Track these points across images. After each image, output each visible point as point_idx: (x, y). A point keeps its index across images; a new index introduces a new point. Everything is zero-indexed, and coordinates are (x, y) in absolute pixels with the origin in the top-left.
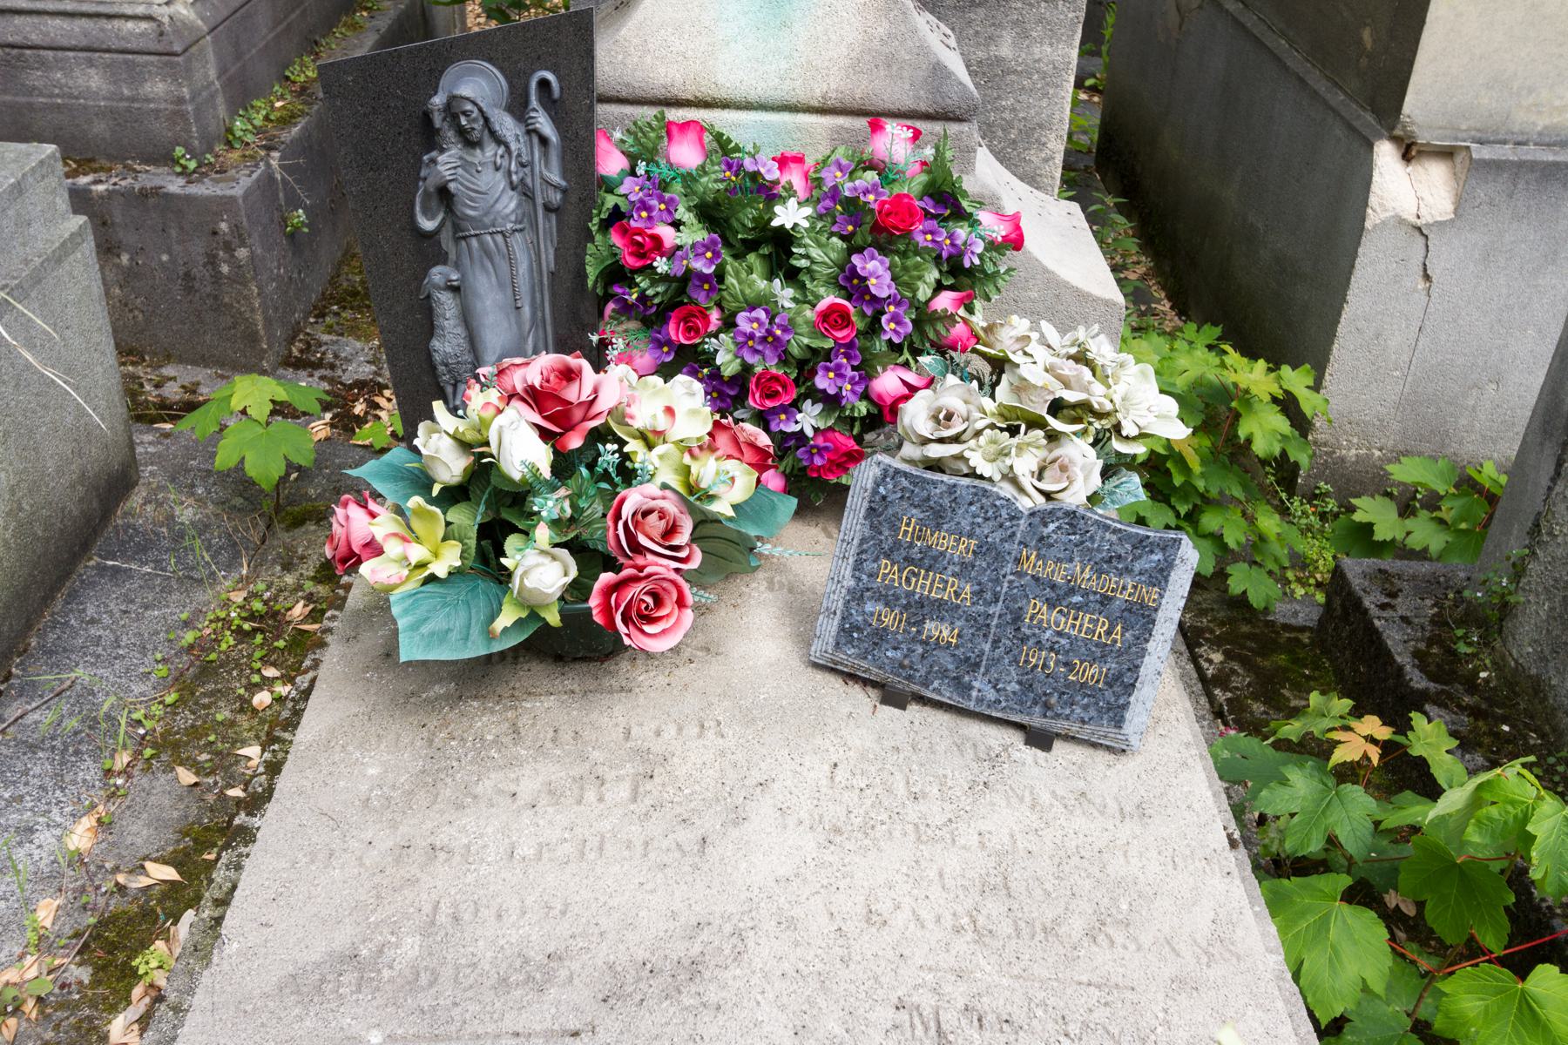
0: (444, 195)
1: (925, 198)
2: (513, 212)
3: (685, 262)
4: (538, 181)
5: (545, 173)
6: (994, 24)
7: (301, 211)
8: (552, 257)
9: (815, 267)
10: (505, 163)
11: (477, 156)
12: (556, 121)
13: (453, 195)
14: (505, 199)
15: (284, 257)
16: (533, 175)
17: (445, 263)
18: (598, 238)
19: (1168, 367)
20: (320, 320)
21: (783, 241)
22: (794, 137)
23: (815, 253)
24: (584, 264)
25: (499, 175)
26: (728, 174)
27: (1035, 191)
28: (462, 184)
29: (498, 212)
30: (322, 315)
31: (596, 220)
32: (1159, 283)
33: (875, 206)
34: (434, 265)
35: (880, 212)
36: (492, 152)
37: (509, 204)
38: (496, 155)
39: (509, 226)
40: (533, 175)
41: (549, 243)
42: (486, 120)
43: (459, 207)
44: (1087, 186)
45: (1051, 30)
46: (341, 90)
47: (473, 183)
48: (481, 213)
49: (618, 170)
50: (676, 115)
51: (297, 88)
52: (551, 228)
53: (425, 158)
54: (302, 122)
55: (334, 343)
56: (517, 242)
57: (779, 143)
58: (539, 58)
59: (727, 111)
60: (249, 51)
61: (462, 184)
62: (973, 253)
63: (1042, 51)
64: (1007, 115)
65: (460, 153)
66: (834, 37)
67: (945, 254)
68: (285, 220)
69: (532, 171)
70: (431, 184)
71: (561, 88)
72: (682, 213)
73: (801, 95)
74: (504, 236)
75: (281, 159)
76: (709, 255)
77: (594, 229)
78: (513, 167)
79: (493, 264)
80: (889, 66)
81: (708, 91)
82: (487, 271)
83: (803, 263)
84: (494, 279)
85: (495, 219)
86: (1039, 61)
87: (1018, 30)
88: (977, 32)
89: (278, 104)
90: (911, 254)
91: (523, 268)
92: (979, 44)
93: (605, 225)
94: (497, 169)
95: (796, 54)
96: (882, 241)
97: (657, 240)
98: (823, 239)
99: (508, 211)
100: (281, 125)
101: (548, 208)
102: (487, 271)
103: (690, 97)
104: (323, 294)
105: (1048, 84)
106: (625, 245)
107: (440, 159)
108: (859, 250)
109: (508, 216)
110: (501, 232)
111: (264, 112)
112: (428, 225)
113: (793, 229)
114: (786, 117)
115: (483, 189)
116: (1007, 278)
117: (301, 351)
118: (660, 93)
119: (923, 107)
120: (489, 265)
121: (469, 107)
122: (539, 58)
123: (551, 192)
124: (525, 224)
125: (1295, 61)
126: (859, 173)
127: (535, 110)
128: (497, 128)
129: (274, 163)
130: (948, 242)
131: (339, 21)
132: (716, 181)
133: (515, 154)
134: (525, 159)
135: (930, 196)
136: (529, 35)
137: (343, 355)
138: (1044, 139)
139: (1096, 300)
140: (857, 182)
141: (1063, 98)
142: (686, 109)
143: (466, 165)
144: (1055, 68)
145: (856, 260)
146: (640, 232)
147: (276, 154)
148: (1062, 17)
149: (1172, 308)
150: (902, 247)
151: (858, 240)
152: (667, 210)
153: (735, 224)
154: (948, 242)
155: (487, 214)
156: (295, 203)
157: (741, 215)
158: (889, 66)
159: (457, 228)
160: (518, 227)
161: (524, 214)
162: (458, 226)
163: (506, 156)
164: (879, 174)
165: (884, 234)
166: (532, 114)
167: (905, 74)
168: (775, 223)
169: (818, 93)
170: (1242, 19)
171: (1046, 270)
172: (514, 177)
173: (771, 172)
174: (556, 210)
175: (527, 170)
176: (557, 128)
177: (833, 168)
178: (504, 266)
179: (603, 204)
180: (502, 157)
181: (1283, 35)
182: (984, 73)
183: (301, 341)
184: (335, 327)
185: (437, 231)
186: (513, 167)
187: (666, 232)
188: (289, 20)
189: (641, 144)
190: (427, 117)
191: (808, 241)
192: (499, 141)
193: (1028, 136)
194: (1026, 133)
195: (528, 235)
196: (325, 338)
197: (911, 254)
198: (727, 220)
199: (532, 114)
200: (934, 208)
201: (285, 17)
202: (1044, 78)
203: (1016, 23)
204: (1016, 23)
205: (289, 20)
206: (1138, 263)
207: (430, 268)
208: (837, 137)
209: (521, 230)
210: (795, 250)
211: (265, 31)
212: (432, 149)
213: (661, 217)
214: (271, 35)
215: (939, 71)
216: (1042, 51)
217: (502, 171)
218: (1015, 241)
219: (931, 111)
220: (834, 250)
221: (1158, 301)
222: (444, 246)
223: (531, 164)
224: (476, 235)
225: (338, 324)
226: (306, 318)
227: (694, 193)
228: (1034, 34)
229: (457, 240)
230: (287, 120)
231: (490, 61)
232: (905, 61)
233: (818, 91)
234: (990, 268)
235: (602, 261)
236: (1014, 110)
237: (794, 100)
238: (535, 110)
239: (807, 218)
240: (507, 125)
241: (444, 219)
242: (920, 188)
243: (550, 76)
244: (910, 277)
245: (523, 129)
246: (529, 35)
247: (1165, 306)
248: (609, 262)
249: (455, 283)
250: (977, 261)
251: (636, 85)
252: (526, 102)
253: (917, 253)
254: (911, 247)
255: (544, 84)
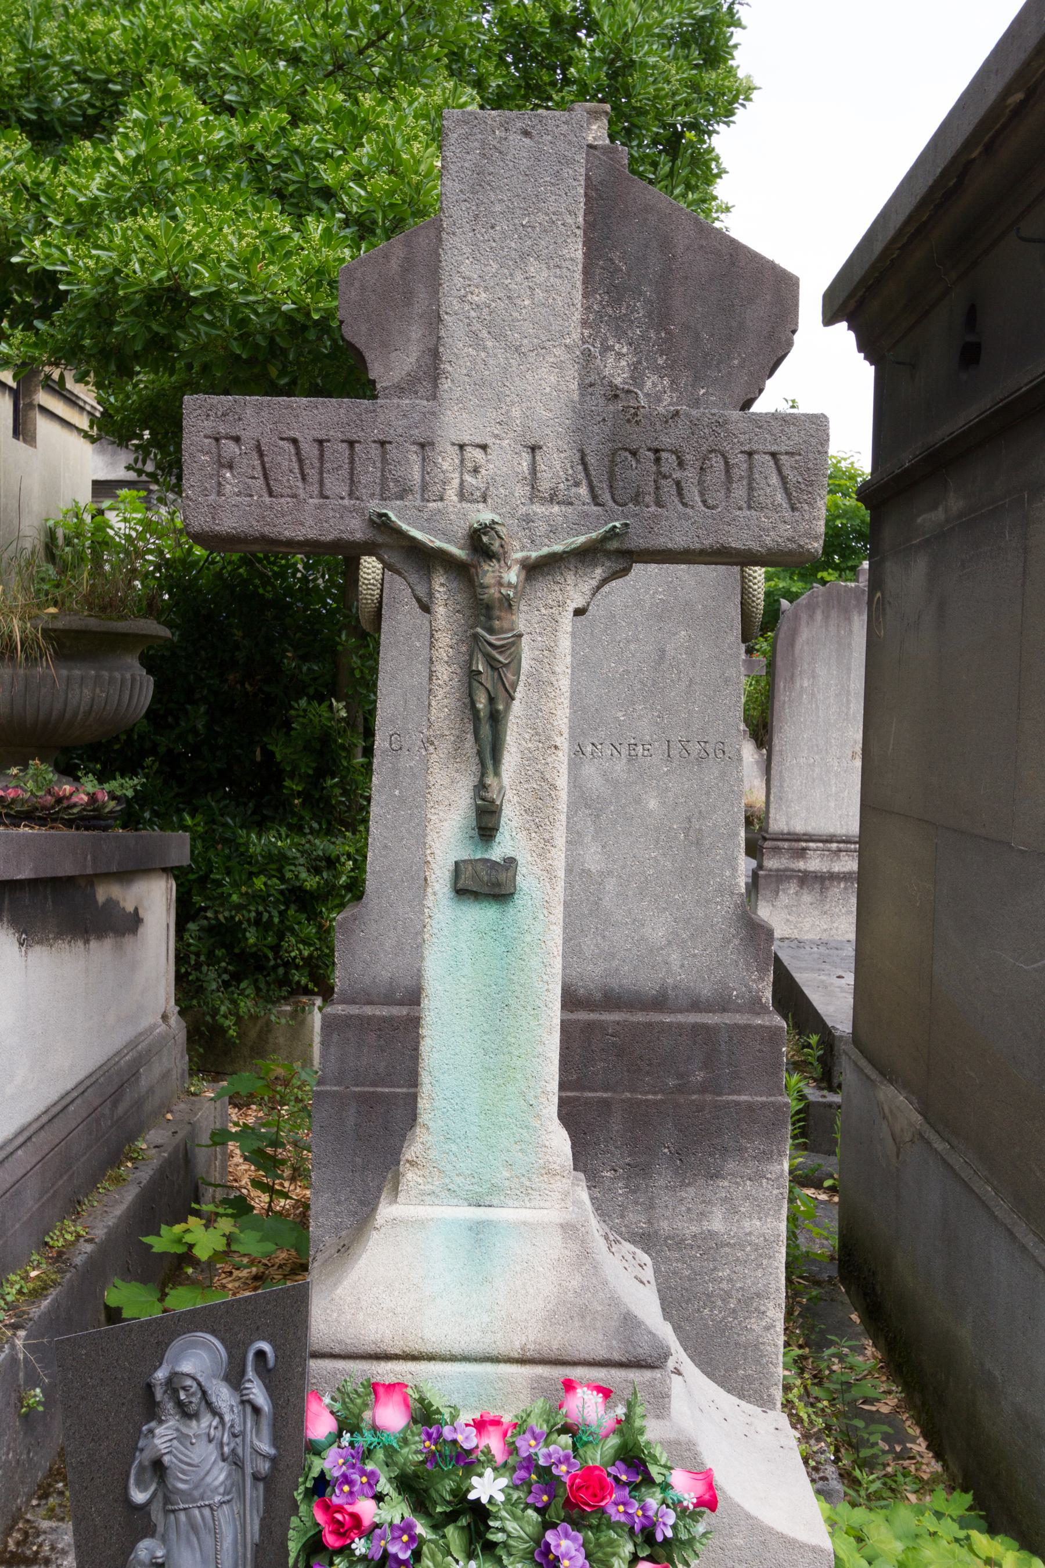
0: (158, 1467)
1: (617, 1463)
2: (221, 1484)
3: (383, 1543)
4: (248, 1450)
5: (256, 1442)
6: (704, 1202)
7: (38, 1390)
8: (257, 1527)
9: (511, 1542)
10: (219, 1434)
11: (194, 1428)
12: (270, 1389)
13: (166, 1468)
14: (215, 1471)
15: (15, 1440)
16: (244, 1445)
17: (152, 1536)
18: (303, 1508)
19: (913, 1559)
20: (43, 1502)
21: (480, 1512)
22: (497, 1386)
23: (511, 1526)
24: (287, 1539)
25: (212, 1446)
26: (427, 1443)
27: (743, 1403)
28: (176, 1457)
29: (209, 1485)
30: (45, 1496)
31: (301, 1489)
32: (912, 1417)
33: (566, 1479)
34: (142, 1538)
35: (571, 1487)
36: (208, 1423)
37: (220, 1475)
38: (210, 1426)
39: (217, 1498)
40: (244, 1445)
41: (255, 1512)
42: (204, 1393)
43: (171, 1480)
44: (832, 1300)
45: (758, 1206)
46: (74, 1363)
47: (190, 1458)
48: (191, 1486)
49: (326, 1433)
50: (386, 1372)
51: (53, 1254)
52: (257, 1497)
53: (145, 1428)
54: (53, 1293)
55: (54, 1530)
56: (224, 1515)
57: (483, 1392)
58: (258, 1328)
59: (433, 1362)
60: (13, 1226)
61: (176, 1457)
62: (665, 1524)
63: (753, 1225)
64: (724, 1285)
65: (177, 1424)
66: (531, 1291)
67: (637, 1527)
68: (21, 1400)
69: (244, 1440)
70: (144, 1458)
71: (276, 1357)
72: (384, 1486)
73: (502, 1347)
74: (212, 1509)
75: (27, 1338)
76: (405, 1538)
77: (299, 1498)
78: (225, 1439)
79: (198, 1539)
80: (583, 1317)
81: (414, 1345)
82: (192, 1548)
83: (499, 1537)
84: (198, 1555)
85: (204, 1492)
86: (750, 1234)
87: (728, 1206)
88: (689, 1209)
89: (33, 1274)
90: (604, 1528)
91: (227, 1543)
92: (691, 1220)
93: (309, 1493)
94: (210, 1441)
95: (496, 1308)
96: (575, 1516)
97: (356, 1518)
98: (519, 1512)
99: (217, 1483)
100: (32, 1299)
101: (256, 1477)
102: (192, 1548)
103: (398, 1352)
104: (51, 1469)
105: (761, 1256)
106: (326, 1523)
107: (157, 1431)
108: (554, 1526)
109: (217, 1488)
110: (209, 1505)
111: (18, 1287)
112: (139, 1497)
113: (490, 1502)
114: (488, 1368)
115: (196, 1460)
116: (704, 1541)
117: (18, 1544)
118: (371, 1349)
119: (616, 1356)
120: (195, 1540)
121: (189, 1382)
122: (258, 1328)
123: (260, 1460)
124: (234, 1494)
125: (1002, 1209)
126: (555, 1436)
127: (250, 1381)
128: (214, 1399)
129: (19, 1343)
130: (640, 1513)
131: (104, 1175)
132: (417, 1452)
133: (228, 1425)
134: (237, 1429)
135: (623, 1460)
136: (250, 1308)
137: (60, 1546)
138: (763, 1308)
139: (803, 1546)
140: (552, 1448)
141: (777, 1268)
142: (395, 1362)
143: (182, 1437)
144: (766, 1240)
145: (550, 1537)
146: (340, 1509)
147: (22, 1333)
148: (767, 1194)
149: (928, 1448)
150: (595, 1522)
151: (552, 1514)
152: (369, 1483)
153: (434, 1495)
154: (640, 1513)
155: (196, 1487)
156: (33, 1381)
157: (440, 1487)
158: (583, 1317)
159: (167, 1500)
160: (227, 1498)
161: (233, 1485)
162: (167, 1497)
163: (220, 1427)
164: (572, 1437)
165: (576, 1510)
166: (248, 1385)
167: (598, 1325)
168: (472, 1496)
169: (517, 1345)
170: (950, 1161)
171: (749, 1516)
172: (226, 1449)
173: (469, 1439)
174: (263, 1479)
175: (239, 1440)
176: (270, 1396)
177: (528, 1436)
178: (209, 1540)
179: (310, 1468)
180: (216, 1428)
181: (988, 1182)
182: (699, 1247)
183: (19, 1530)
184: (58, 1510)
185: (149, 1502)
186: (225, 1439)
187: (366, 1508)
188: (55, 1188)
189: (348, 1408)
190: (149, 1387)
191: (504, 1514)
192: (215, 1412)
193: (747, 1306)
194: (745, 1302)
195: (236, 1507)
196: (45, 1525)
197: (604, 1528)
198: (426, 1491)
199: (248, 1385)
200: (626, 1473)
201: (53, 1185)
202: (756, 1250)
203: (725, 1200)
204: (725, 1200)
205: (55, 1188)
206: (890, 1392)
207: (138, 1541)
208: (538, 1387)
209: (229, 1501)
210: (491, 1524)
211: (31, 1203)
212: (152, 1420)
213: (362, 1490)
214: (37, 1206)
215: (629, 1322)
216: (753, 1225)
217: (214, 1442)
218: (709, 1502)
219: (624, 1359)
220: (528, 1522)
221: (913, 1440)
222: (153, 1518)
223: (243, 1433)
224: (185, 1509)
225: (60, 1505)
226: (29, 1500)
227: (396, 1464)
228: (743, 1210)
229: (167, 1512)
230: (37, 1294)
231: (213, 1332)
232: (597, 1311)
233: (517, 1343)
234: (684, 1536)
235: (306, 1533)
236: (730, 1280)
237: (495, 1353)
238: (250, 1381)
239: (502, 1490)
240: (223, 1396)
241: (156, 1490)
242: (612, 1451)
243: (266, 1347)
244: (605, 1554)
245: (238, 1399)
246: (250, 1308)
247: (920, 1446)
248: (312, 1533)
249: (160, 1560)
250: (669, 1533)
251: (348, 1341)
252: (243, 1372)
253: (611, 1526)
254: (604, 1521)
255: (261, 1354)
